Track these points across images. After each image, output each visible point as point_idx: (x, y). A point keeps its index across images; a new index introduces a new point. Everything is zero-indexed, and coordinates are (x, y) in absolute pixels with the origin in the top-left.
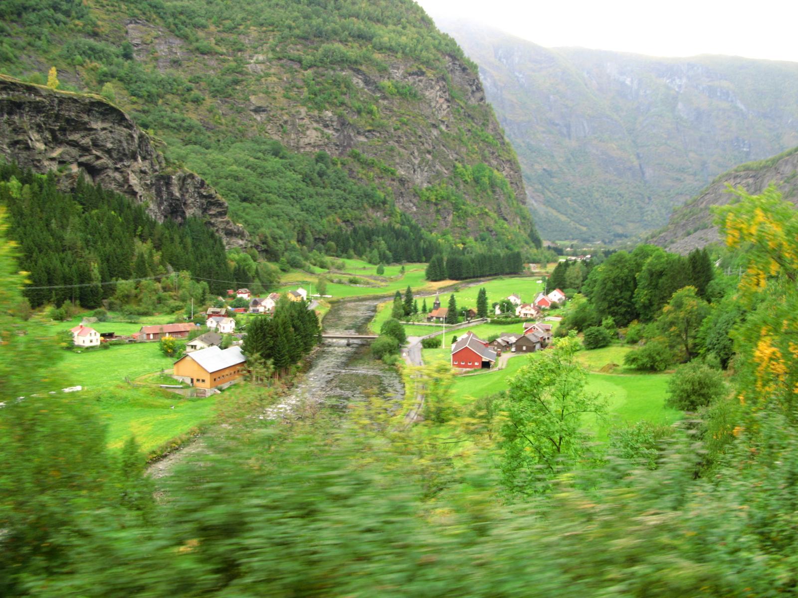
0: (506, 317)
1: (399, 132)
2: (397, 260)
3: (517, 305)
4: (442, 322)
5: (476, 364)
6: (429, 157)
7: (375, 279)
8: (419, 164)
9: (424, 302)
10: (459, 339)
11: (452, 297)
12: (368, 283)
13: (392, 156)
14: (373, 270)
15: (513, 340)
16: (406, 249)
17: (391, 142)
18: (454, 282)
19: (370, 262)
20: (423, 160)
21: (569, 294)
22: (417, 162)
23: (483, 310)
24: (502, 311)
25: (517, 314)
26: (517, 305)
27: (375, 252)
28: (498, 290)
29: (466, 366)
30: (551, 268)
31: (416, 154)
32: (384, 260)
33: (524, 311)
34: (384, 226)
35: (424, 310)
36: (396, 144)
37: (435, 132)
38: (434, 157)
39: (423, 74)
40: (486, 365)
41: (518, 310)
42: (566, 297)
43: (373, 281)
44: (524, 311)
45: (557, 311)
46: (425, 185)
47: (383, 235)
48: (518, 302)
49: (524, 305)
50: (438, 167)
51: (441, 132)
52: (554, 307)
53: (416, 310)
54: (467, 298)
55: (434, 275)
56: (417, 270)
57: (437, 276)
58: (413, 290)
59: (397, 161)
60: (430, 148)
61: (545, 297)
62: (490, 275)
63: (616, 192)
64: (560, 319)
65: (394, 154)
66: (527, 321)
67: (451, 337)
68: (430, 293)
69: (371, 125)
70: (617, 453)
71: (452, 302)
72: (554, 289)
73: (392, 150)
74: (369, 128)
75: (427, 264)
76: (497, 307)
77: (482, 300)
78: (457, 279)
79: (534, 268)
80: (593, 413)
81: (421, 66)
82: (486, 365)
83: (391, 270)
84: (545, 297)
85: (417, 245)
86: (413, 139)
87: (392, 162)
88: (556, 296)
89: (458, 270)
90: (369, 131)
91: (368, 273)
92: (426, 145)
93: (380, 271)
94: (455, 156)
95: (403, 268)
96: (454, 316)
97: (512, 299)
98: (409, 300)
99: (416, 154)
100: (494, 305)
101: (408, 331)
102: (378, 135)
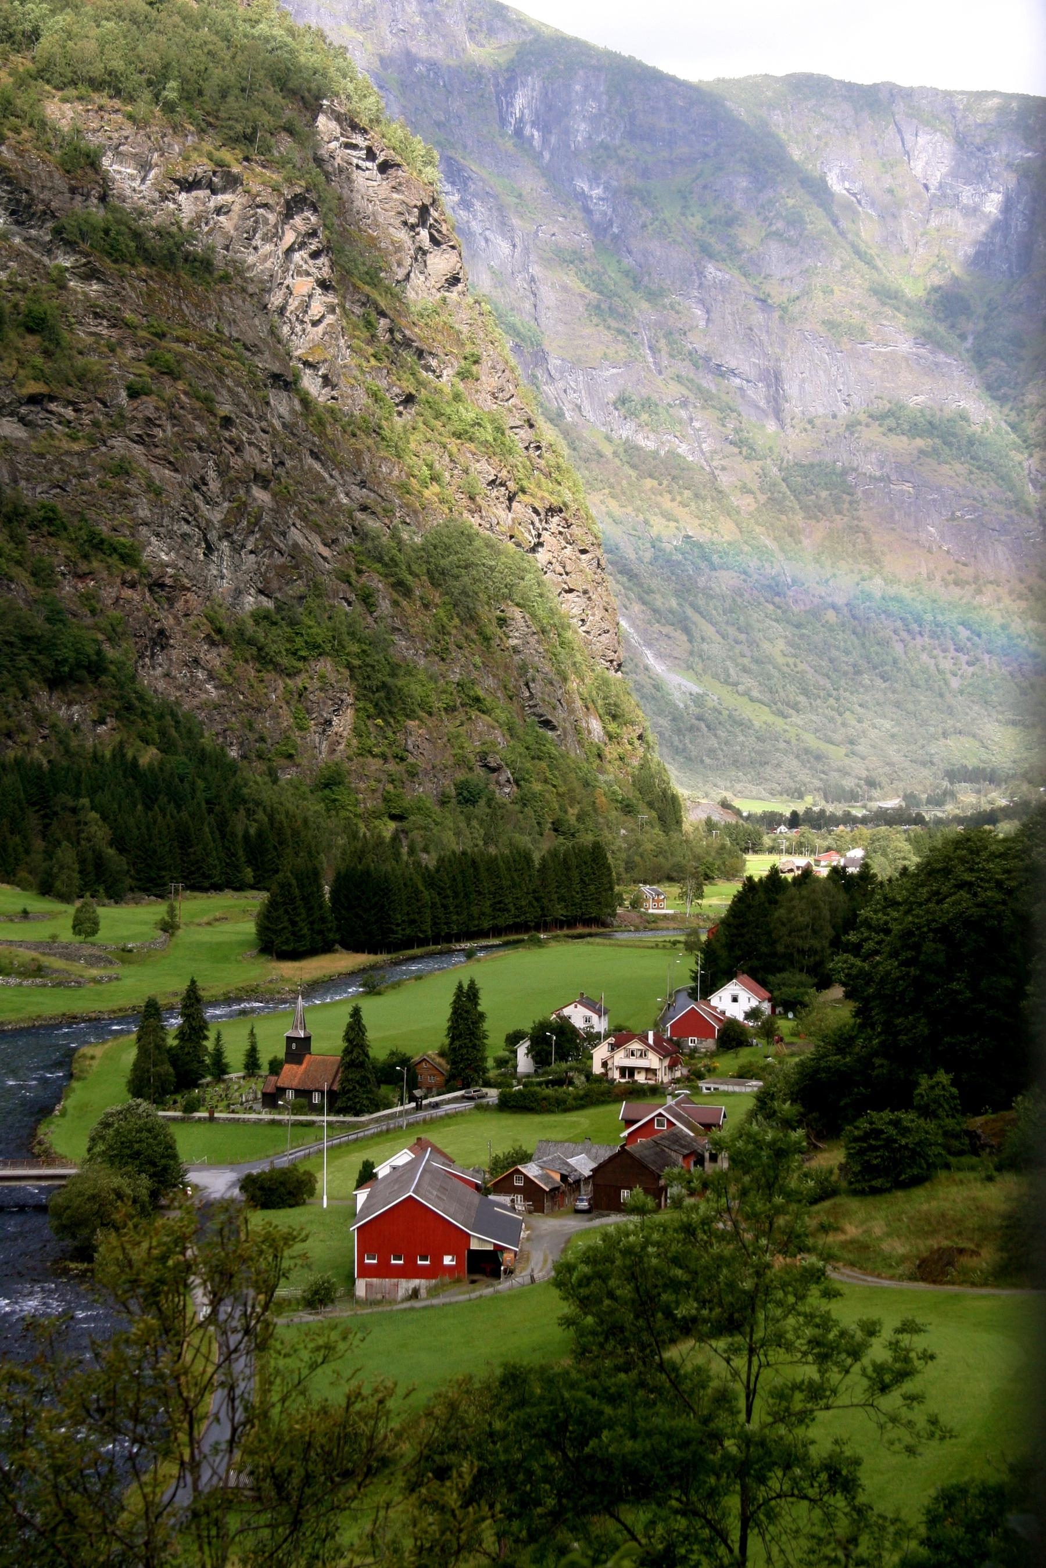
0: (559, 1082)
1: (148, 406)
2: (151, 883)
3: (594, 1039)
4: (318, 1110)
5: (448, 1260)
6: (261, 496)
7: (68, 955)
8: (225, 523)
9: (252, 1034)
10: (382, 1171)
11: (356, 1013)
12: (39, 971)
13: (125, 494)
14: (57, 919)
15: (583, 1164)
16: (184, 839)
17: (118, 442)
18: (363, 959)
19: (46, 889)
20: (241, 509)
21: (788, 992)
22: (216, 516)
23: (464, 1057)
24: (540, 1057)
25: (597, 1069)
26: (594, 1039)
27: (66, 854)
28: (522, 982)
29: (409, 1271)
30: (719, 898)
31: (214, 486)
32: (100, 881)
33: (621, 1059)
34: (96, 758)
35: (252, 1064)
36: (138, 450)
37: (282, 405)
38: (284, 499)
39: (232, 182)
40: (486, 1265)
41: (600, 1053)
42: (774, 1002)
43: (58, 963)
44: (621, 1059)
45: (744, 1056)
46: (250, 601)
47: (93, 791)
48: (600, 1025)
49: (620, 1037)
50: (296, 535)
51: (306, 402)
52: (731, 1036)
53: (220, 1069)
54: (410, 1013)
55: (278, 941)
56: (223, 921)
57: (298, 937)
58: (210, 987)
59: (144, 512)
60: (265, 465)
61: (700, 1008)
62: (497, 931)
63: (953, 617)
64: (754, 1085)
65: (133, 487)
66: (635, 1092)
67: (355, 1160)
68: (274, 998)
69: (39, 376)
70: (58, 554)
71: (356, 1029)
72: (729, 976)
73: (123, 470)
74: (34, 387)
75: (265, 895)
76: (522, 1049)
77: (466, 1010)
78: (373, 951)
79: (663, 902)
80: (860, 1414)
81: (226, 155)
82: (486, 1265)
83: (128, 920)
84: (700, 1008)
85: (222, 825)
86: (201, 430)
87: (122, 518)
88: (735, 1001)
89: (361, 909)
90: (34, 400)
91: (38, 931)
92: (251, 454)
93: (86, 926)
94: (358, 493)
95: (172, 911)
96: (365, 1083)
97: (578, 1016)
98: (195, 1030)
99: (214, 486)
100: (514, 1039)
101: (188, 1141)
102: (69, 413)
